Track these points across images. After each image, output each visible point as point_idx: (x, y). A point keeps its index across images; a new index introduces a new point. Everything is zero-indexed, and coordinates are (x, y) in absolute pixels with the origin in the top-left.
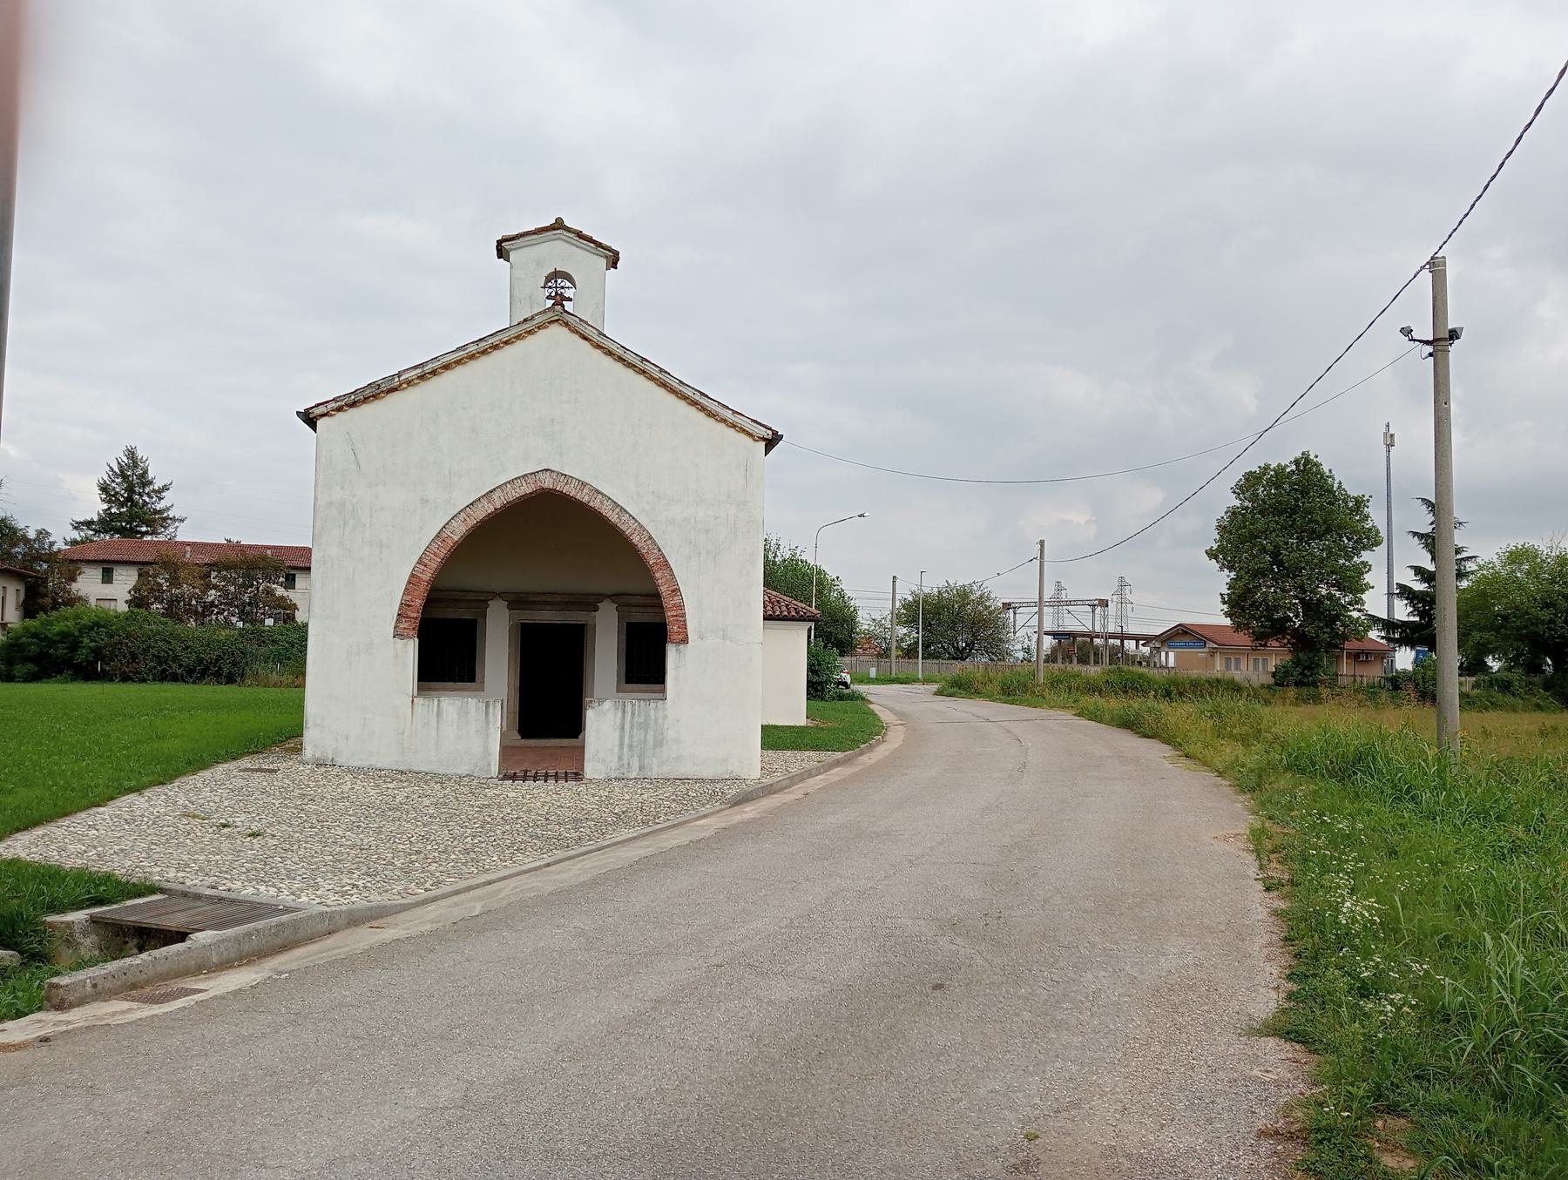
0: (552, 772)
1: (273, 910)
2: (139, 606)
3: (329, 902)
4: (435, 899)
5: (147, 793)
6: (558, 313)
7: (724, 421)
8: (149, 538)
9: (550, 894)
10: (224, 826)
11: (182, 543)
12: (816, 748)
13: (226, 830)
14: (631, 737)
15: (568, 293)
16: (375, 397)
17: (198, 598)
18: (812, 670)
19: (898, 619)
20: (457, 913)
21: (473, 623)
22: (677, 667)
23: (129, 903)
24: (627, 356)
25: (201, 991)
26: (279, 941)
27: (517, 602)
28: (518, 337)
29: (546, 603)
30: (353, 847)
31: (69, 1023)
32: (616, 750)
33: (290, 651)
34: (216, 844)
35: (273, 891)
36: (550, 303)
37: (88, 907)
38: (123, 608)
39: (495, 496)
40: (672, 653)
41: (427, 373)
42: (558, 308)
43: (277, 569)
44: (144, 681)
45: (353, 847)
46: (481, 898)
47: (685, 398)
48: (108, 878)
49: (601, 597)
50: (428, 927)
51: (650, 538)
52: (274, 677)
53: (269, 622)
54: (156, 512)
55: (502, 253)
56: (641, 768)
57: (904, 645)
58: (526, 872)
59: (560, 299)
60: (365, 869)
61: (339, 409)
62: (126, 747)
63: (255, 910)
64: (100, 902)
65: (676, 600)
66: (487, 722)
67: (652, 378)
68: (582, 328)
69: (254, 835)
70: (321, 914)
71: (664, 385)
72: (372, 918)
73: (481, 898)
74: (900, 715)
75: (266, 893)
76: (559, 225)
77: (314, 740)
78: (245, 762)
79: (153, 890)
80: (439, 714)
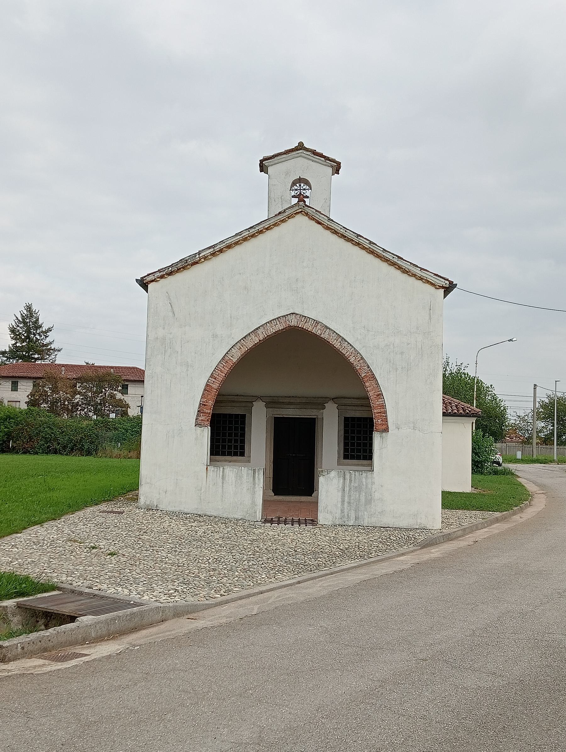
0: (296, 519)
1: (127, 604)
2: (33, 405)
3: (161, 600)
4: (227, 602)
5: (45, 525)
6: (302, 208)
7: (414, 275)
8: (39, 362)
9: (302, 602)
10: (93, 548)
11: (59, 365)
12: (480, 509)
13: (94, 551)
15: (308, 193)
16: (184, 268)
17: (69, 400)
18: (475, 452)
19: (538, 416)
20: (242, 612)
21: (244, 416)
22: (381, 449)
23: (39, 596)
24: (347, 234)
25: (86, 655)
26: (132, 625)
27: (272, 402)
28: (276, 225)
29: (290, 403)
30: (173, 564)
31: (9, 671)
32: (339, 505)
33: (130, 434)
34: (89, 559)
35: (126, 592)
36: (295, 200)
37: (15, 597)
38: (24, 407)
39: (259, 332)
40: (377, 439)
41: (216, 251)
42: (301, 203)
43: (117, 381)
44: (37, 453)
45: (173, 564)
46: (256, 603)
47: (386, 260)
48: (27, 579)
49: (326, 399)
50: (224, 620)
51: (362, 358)
52: (116, 452)
53: (113, 416)
54: (44, 345)
55: (263, 168)
56: (357, 518)
57: (542, 435)
58: (285, 586)
59: (301, 198)
60: (181, 579)
61: (162, 277)
62: (31, 496)
63: (117, 604)
64: (22, 594)
65: (380, 402)
66: (254, 484)
67: (364, 248)
68: (317, 216)
69: (112, 554)
70: (157, 608)
71: (372, 252)
72: (188, 613)
73: (256, 603)
74: (542, 486)
75: (122, 593)
76: (301, 147)
77: (146, 493)
78: (103, 507)
79: (54, 588)
80: (223, 477)
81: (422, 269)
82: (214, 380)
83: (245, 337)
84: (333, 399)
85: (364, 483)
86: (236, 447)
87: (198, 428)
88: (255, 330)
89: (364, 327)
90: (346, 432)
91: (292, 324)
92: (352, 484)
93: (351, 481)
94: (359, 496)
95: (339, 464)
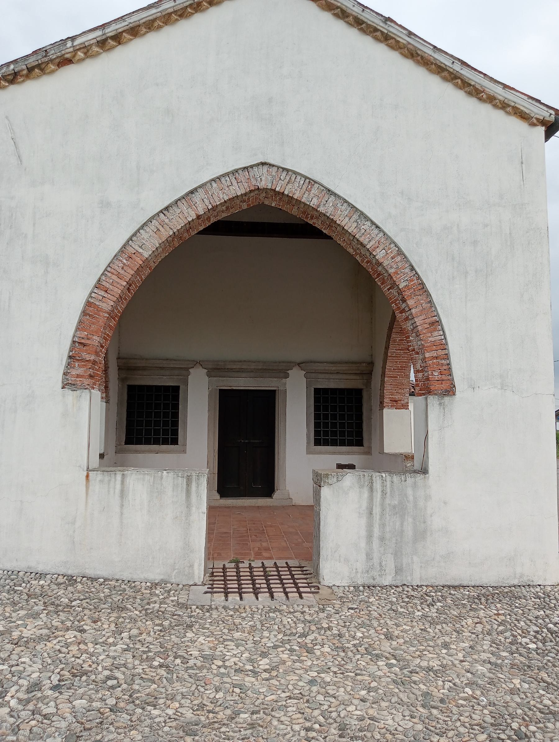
14: (383, 525)
21: (176, 389)
24: (366, 16)
27: (216, 369)
32: (363, 544)
39: (197, 198)
51: (400, 252)
56: (399, 570)
65: (436, 336)
66: (189, 506)
80: (123, 494)
81: (505, 86)
82: (103, 293)
83: (167, 208)
84: (299, 364)
85: (411, 498)
86: (166, 432)
87: (67, 391)
88: (187, 194)
89: (402, 193)
90: (317, 408)
91: (262, 185)
92: (388, 501)
93: (384, 493)
94: (402, 525)
95: (309, 452)
